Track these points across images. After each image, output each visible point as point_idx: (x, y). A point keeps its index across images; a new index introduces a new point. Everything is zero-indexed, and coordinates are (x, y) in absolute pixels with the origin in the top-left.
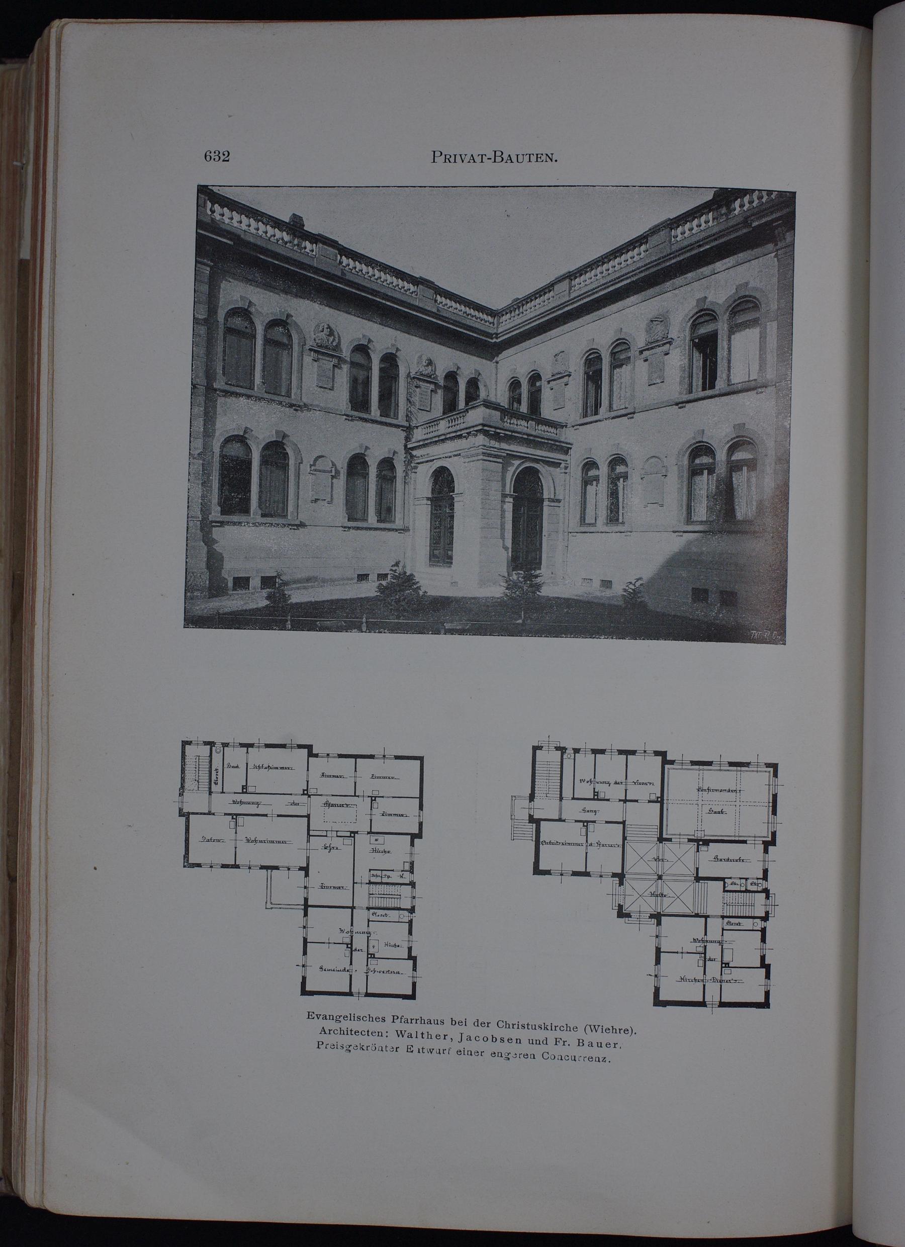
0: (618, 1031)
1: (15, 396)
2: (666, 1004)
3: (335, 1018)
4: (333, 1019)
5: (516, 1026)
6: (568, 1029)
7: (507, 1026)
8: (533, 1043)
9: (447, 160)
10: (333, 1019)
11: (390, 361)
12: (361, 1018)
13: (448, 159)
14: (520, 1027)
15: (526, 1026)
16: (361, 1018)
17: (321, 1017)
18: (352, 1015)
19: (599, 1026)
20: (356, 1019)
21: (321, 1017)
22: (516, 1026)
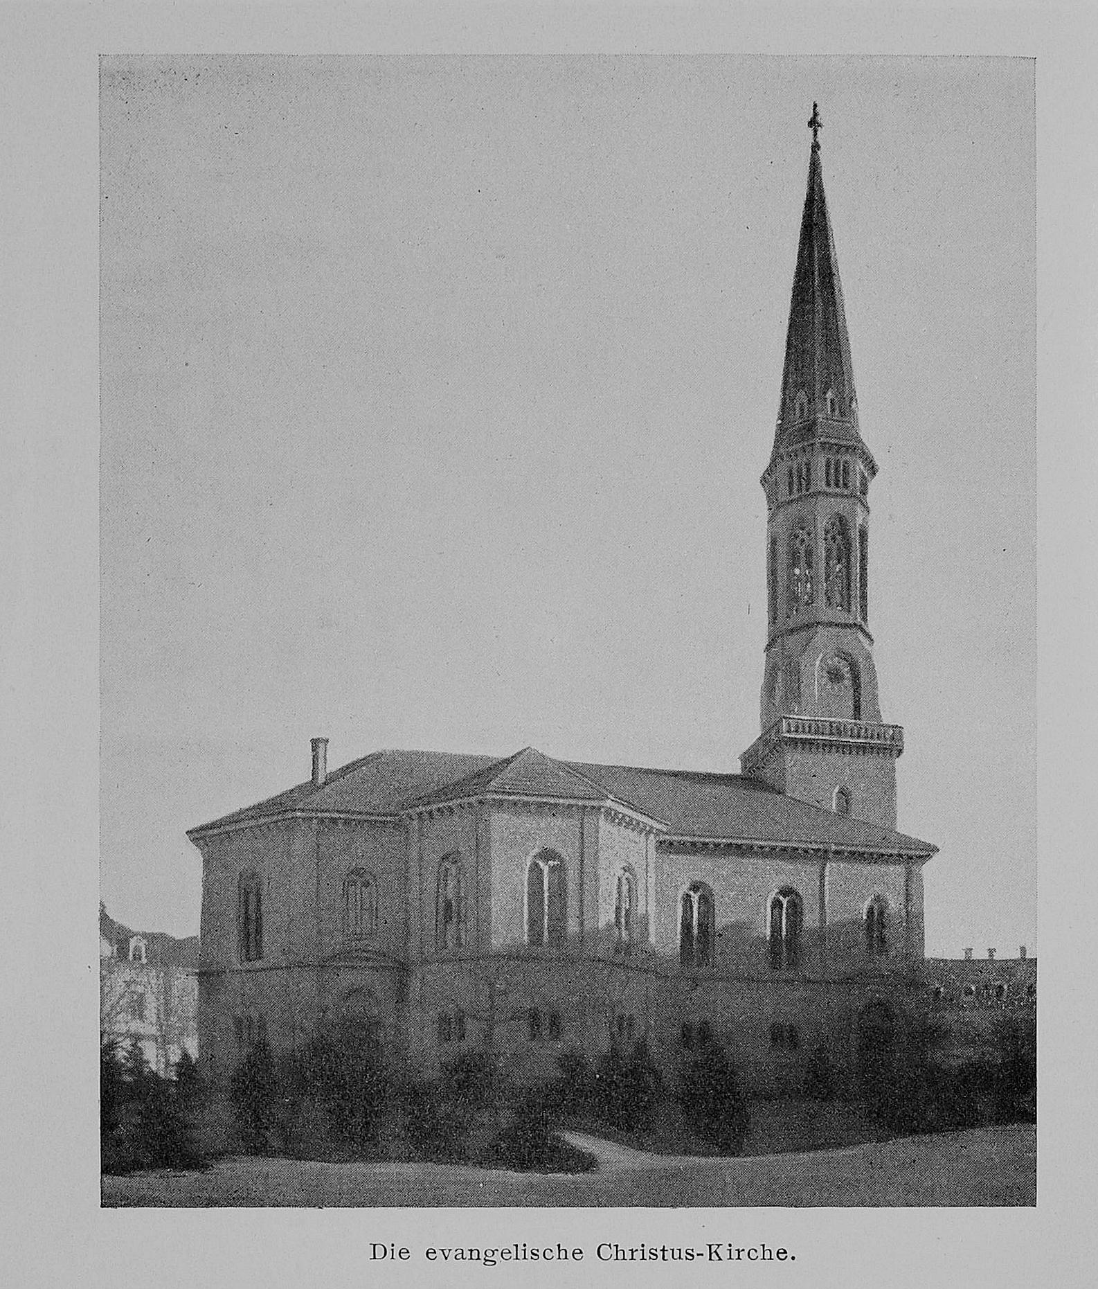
0: (628, 1255)
1: (707, 840)
2: (315, 749)
3: (482, 1256)
4: (478, 1259)
5: (638, 1255)
6: (563, 1256)
7: (620, 1256)
8: (471, 1251)
9: (714, 1255)
10: (478, 1259)
11: (828, 484)
12: (540, 1254)
13: (715, 1252)
14: (647, 1255)
15: (660, 1254)
16: (540, 1254)
17: (453, 1253)
18: (521, 1247)
19: (450, 1250)
20: (529, 1255)
21: (453, 1253)
22: (638, 1255)
